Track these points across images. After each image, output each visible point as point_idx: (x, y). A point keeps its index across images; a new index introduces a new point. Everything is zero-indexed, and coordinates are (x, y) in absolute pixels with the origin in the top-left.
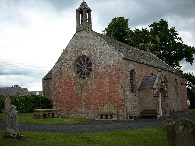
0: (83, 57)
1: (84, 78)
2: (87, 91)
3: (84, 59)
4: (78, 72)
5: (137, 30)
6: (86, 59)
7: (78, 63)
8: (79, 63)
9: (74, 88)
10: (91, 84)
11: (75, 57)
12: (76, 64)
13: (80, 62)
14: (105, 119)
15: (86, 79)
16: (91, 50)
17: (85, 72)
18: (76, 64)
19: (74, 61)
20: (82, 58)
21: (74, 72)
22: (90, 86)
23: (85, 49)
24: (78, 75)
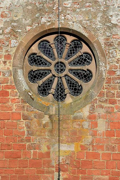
0: (61, 33)
1: (60, 96)
2: (76, 137)
3: (75, 47)
4: (33, 77)
5: (118, 7)
6: (85, 49)
7: (35, 49)
8: (39, 48)
9: (23, 124)
10: (92, 117)
11: (30, 29)
12: (30, 52)
13: (46, 48)
14: (107, 152)
15: (69, 100)
16: (96, 17)
17: (64, 80)
18: (30, 52)
19: (25, 39)
20: (54, 36)
21: (22, 76)
22: (86, 125)
23: (74, 11)
24: (35, 86)
